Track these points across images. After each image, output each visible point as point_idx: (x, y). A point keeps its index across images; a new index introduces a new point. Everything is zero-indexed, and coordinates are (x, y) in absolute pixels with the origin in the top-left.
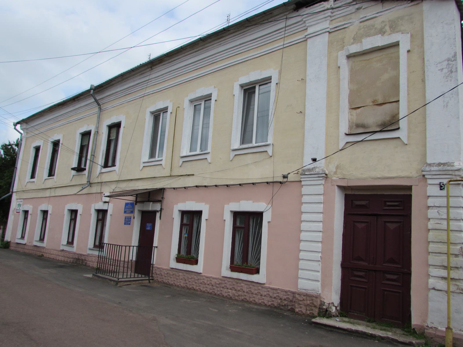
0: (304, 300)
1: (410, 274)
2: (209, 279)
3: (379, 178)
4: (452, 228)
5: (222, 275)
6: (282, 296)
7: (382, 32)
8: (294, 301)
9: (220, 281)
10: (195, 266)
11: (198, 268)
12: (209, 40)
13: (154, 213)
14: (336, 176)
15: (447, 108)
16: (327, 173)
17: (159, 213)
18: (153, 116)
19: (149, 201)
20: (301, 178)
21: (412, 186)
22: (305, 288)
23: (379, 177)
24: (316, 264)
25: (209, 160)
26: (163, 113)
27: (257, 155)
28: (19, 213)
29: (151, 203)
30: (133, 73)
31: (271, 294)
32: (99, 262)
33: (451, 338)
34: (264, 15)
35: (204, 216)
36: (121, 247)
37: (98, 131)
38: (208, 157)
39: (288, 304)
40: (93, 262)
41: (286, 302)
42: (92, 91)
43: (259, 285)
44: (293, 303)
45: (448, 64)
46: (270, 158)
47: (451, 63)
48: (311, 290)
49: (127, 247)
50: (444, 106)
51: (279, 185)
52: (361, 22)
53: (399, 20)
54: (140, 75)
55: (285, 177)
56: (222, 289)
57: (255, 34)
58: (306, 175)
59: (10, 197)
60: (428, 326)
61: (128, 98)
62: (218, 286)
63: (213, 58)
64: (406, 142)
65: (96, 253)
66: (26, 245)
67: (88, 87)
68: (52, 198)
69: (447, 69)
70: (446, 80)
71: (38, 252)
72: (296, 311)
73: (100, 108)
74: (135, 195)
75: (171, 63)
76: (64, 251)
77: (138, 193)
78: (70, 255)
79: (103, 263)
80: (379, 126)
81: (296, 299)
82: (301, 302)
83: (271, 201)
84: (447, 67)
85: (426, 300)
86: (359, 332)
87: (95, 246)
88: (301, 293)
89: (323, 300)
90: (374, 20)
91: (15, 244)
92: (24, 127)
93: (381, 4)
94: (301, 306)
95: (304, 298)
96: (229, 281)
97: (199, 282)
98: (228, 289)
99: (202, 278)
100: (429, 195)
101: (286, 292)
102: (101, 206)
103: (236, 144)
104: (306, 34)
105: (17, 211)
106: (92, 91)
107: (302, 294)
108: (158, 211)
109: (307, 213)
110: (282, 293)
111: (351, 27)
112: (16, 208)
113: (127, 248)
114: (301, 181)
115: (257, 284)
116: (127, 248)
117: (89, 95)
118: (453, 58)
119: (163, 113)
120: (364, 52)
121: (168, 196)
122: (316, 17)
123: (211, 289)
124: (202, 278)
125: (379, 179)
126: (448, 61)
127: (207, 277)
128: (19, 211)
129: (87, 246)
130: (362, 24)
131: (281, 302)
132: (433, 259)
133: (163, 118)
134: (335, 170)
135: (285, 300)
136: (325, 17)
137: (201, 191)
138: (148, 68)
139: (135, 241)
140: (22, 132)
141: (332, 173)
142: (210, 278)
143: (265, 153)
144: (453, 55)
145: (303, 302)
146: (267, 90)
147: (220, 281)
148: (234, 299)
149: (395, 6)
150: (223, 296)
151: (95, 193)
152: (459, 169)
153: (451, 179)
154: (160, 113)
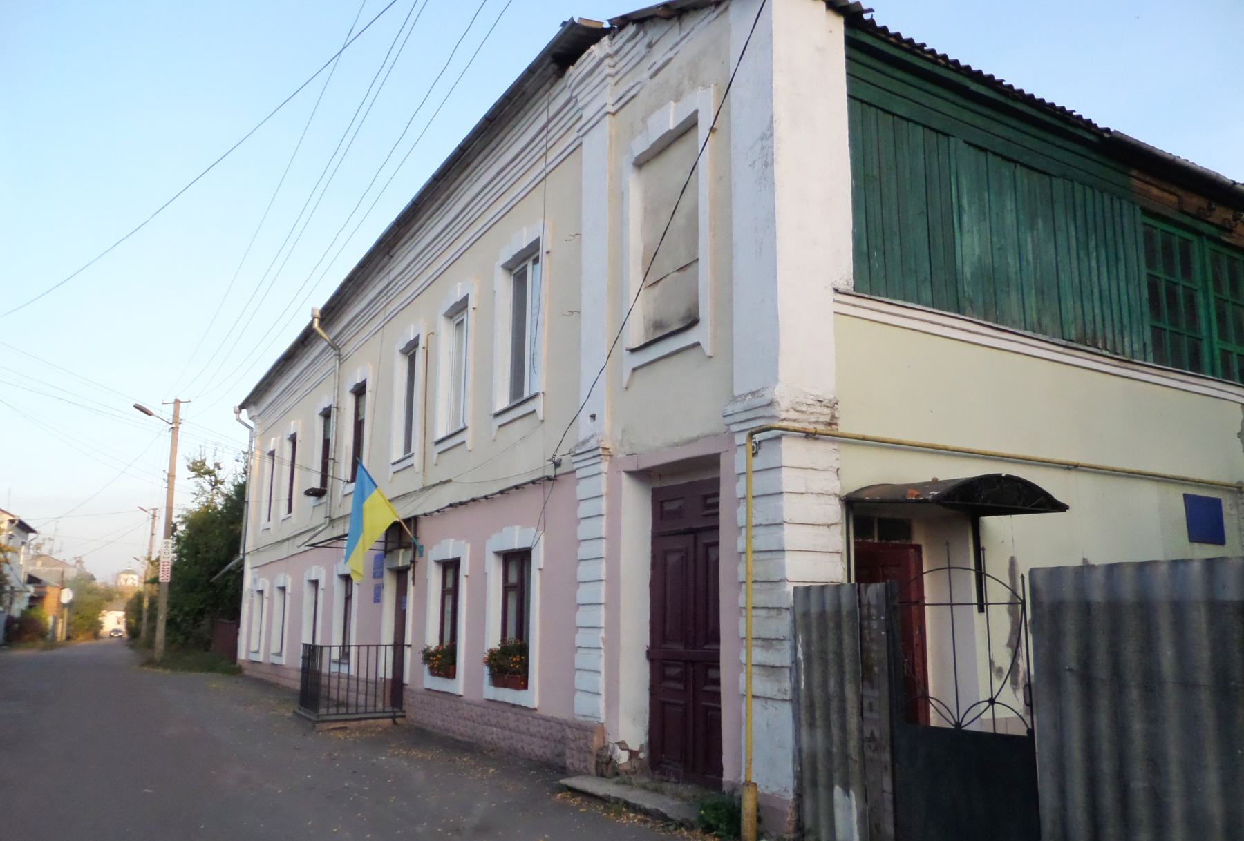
10: (523, 692)
11: (531, 697)
17: (412, 570)
18: (512, 277)
20: (574, 463)
25: (707, 348)
37: (339, 405)
38: (537, 404)
49: (361, 647)
54: (379, 272)
58: (578, 454)
59: (241, 565)
63: (450, 231)
71: (494, 729)
73: (340, 355)
75: (415, 238)
80: (683, 319)
83: (543, 524)
111: (642, 94)
113: (373, 650)
116: (373, 650)
121: (426, 531)
122: (590, 83)
125: (678, 446)
138: (384, 257)
140: (251, 423)
142: (549, 721)
154: (526, 265)
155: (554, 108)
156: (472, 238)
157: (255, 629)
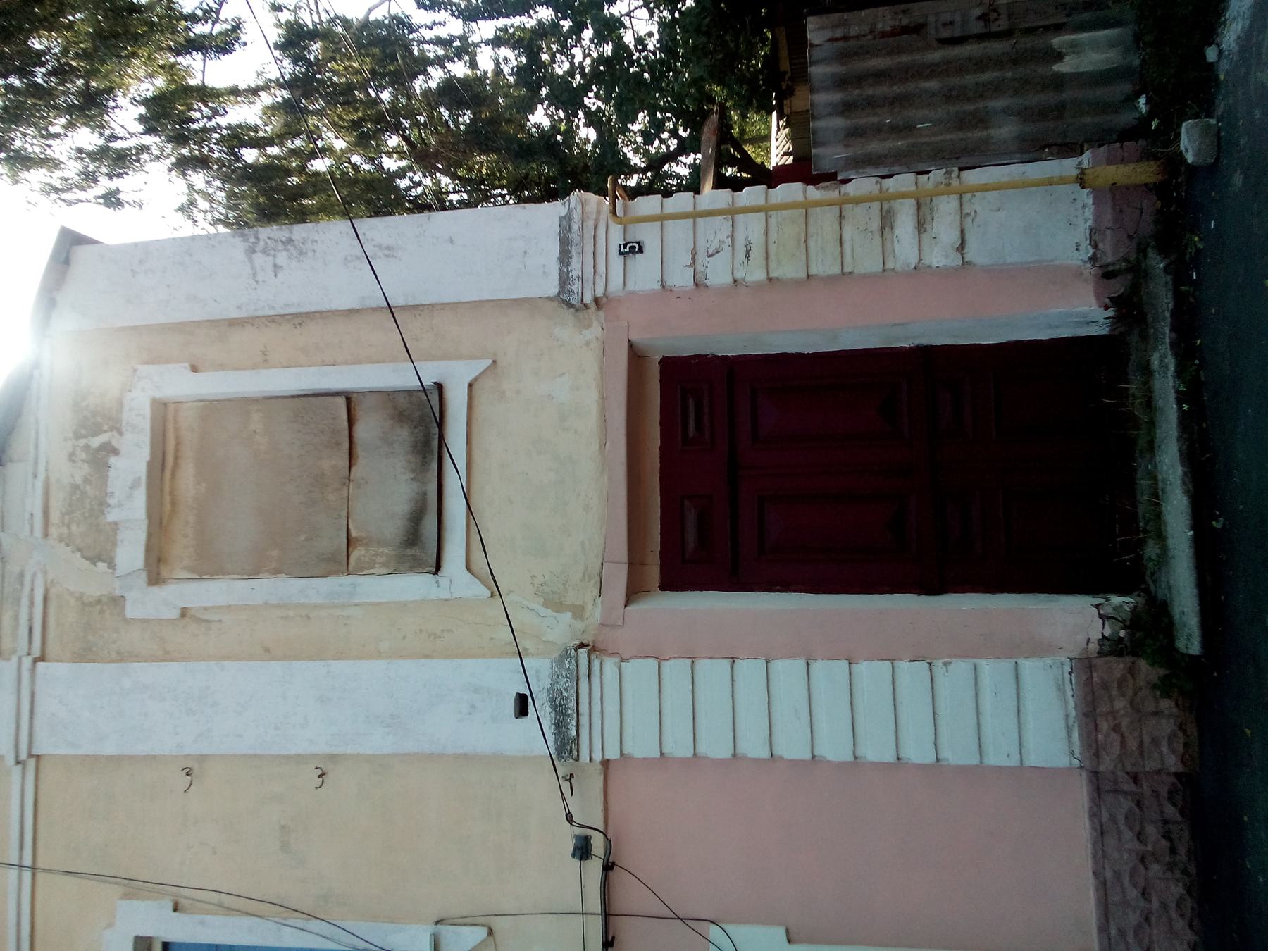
3: (600, 447)
6: (1126, 856)
14: (589, 606)
15: (393, 248)
22: (1064, 733)
23: (597, 447)
31: (1133, 918)
33: (1112, 168)
41: (1152, 831)
46: (493, 937)
47: (262, 243)
48: (1066, 702)
50: (387, 256)
51: (615, 875)
55: (583, 850)
60: (1093, 259)
64: (490, 362)
69: (279, 254)
70: (310, 254)
80: (424, 464)
82: (1132, 744)
84: (272, 252)
85: (1001, 274)
86: (1184, 447)
88: (1090, 746)
89: (1094, 647)
93: (9, 466)
94: (1147, 739)
95: (1104, 726)
107: (1093, 737)
114: (606, 763)
126: (254, 251)
131: (1157, 861)
134: (566, 617)
135: (1140, 836)
141: (579, 625)
144: (241, 239)
145: (1126, 734)
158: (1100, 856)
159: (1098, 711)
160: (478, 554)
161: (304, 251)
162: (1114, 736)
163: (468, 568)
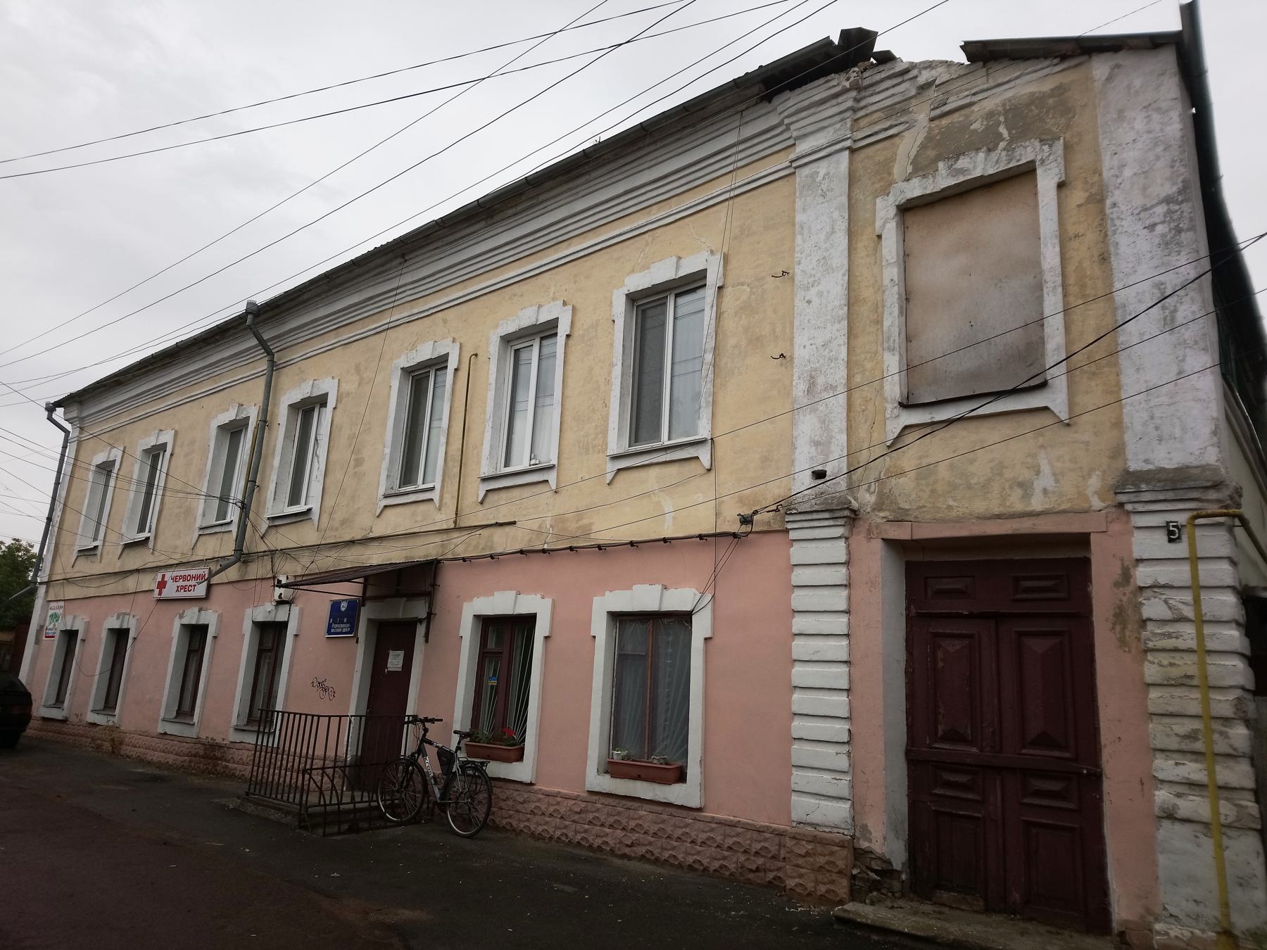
0: (807, 854)
1: (1096, 778)
2: (551, 800)
3: (997, 515)
4: (1210, 645)
5: (589, 787)
6: (748, 842)
7: (988, 142)
8: (782, 856)
9: (583, 805)
12: (549, 184)
13: (412, 624)
14: (882, 514)
16: (856, 509)
17: (424, 625)
19: (398, 595)
20: (787, 522)
21: (1088, 534)
23: (997, 513)
24: (831, 750)
25: (553, 485)
26: (436, 370)
27: (673, 469)
28: (53, 637)
29: (405, 599)
30: (357, 271)
32: (256, 762)
34: (687, 113)
35: (541, 630)
36: (316, 718)
39: (764, 865)
40: (243, 764)
41: (760, 861)
42: (250, 317)
43: (684, 813)
44: (780, 864)
45: (1170, 212)
47: (1177, 207)
50: (1165, 319)
52: (932, 120)
53: (1033, 108)
55: (746, 520)
56: (586, 826)
57: (661, 164)
61: (346, 335)
62: (576, 817)
65: (251, 739)
66: (68, 722)
67: (241, 308)
68: (139, 595)
69: (1166, 225)
72: (788, 887)
74: (361, 580)
76: (167, 737)
77: (370, 573)
78: (184, 747)
79: (272, 766)
81: (788, 852)
82: (800, 861)
87: (250, 719)
90: (967, 111)
91: (40, 722)
92: (74, 414)
94: (803, 871)
96: (606, 803)
97: (526, 809)
98: (602, 825)
99: (533, 797)
100: (1139, 558)
101: (759, 831)
102: (265, 611)
103: (617, 441)
104: (792, 156)
105: (48, 633)
106: (250, 317)
107: (803, 838)
108: (421, 621)
109: (807, 614)
110: (749, 835)
112: (45, 624)
113: (335, 721)
115: (682, 811)
116: (335, 721)
117: (245, 329)
118: (1180, 195)
119: (436, 370)
120: (945, 194)
121: (451, 581)
123: (557, 828)
124: (533, 797)
126: (1168, 203)
127: (548, 795)
128: (54, 633)
129: (230, 722)
130: (937, 122)
132: (1158, 733)
133: (437, 385)
136: (841, 112)
137: (536, 565)
138: (396, 258)
139: (353, 702)
140: (68, 426)
143: (693, 464)
146: (697, 306)
147: (583, 805)
148: (619, 853)
149: (1019, 73)
150: (591, 846)
151: (254, 579)
152: (1220, 484)
153: (1200, 512)
154: (429, 371)
155: (748, 131)
156: (493, 285)
157: (517, 664)
158: (748, 828)
159: (818, 845)
160: (917, 434)
161: (1169, 247)
162: (805, 851)
163: (906, 427)
